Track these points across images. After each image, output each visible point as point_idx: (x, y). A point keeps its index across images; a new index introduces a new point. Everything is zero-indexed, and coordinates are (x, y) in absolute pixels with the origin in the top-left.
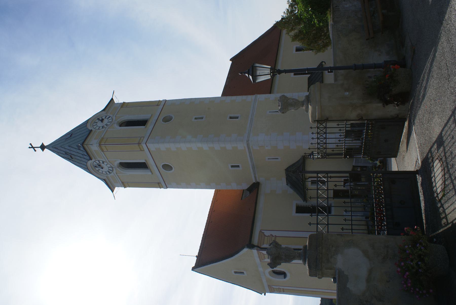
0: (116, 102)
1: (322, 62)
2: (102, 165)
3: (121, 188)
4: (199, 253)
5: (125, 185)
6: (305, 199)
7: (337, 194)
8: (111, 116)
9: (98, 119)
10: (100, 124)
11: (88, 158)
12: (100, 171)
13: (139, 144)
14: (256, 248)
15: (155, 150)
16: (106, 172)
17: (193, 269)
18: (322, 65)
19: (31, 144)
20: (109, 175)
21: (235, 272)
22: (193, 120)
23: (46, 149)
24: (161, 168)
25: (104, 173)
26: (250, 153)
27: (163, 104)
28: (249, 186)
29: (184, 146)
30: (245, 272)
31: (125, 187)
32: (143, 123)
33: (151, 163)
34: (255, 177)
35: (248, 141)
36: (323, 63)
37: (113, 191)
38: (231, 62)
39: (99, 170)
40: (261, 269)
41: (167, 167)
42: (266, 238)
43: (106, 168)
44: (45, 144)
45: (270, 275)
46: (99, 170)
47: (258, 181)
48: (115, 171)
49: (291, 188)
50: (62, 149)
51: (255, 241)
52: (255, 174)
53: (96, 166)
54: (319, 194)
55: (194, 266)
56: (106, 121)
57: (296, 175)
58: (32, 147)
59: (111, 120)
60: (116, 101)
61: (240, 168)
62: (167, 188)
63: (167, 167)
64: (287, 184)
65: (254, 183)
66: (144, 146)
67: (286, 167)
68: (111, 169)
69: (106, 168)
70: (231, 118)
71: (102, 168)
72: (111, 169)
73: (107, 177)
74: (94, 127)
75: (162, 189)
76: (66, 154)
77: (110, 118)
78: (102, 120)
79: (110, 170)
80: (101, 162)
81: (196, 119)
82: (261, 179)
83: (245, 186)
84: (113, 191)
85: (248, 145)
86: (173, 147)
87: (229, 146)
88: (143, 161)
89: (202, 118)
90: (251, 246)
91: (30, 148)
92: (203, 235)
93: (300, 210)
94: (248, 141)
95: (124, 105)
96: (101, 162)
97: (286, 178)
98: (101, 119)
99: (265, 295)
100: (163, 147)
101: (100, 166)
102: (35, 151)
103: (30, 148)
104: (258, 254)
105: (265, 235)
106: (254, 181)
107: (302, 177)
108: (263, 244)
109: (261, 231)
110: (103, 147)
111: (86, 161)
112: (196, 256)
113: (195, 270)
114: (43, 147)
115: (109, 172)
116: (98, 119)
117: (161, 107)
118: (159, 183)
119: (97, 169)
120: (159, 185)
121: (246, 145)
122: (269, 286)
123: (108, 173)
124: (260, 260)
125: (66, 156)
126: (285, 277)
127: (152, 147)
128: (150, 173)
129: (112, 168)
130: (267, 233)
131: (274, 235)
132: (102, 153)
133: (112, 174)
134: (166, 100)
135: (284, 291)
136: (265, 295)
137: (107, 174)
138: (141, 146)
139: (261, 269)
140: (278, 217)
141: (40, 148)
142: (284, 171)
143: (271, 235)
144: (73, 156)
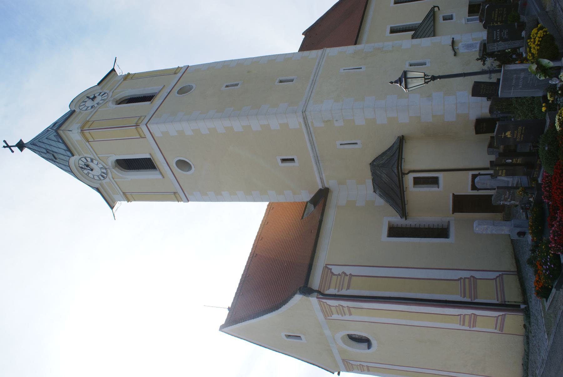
0: (119, 75)
1: (435, 7)
2: (92, 165)
3: (122, 202)
4: (233, 303)
5: (128, 197)
6: (404, 214)
7: (461, 204)
8: (107, 91)
9: (88, 97)
10: (89, 103)
11: (69, 153)
12: (90, 175)
13: (137, 125)
14: (316, 294)
15: (160, 135)
16: (98, 176)
17: (222, 328)
18: (434, 12)
19: (5, 141)
20: (104, 181)
21: (288, 336)
22: (224, 88)
23: (26, 150)
24: (176, 167)
25: (96, 178)
26: (309, 134)
27: (183, 70)
28: (312, 195)
29: (204, 126)
30: (302, 336)
31: (128, 200)
32: (148, 98)
33: (158, 159)
34: (321, 179)
35: (304, 112)
36: (436, 9)
37: (112, 208)
38: (304, 36)
39: (89, 173)
40: (327, 332)
41: (183, 165)
42: (334, 278)
43: (97, 171)
44: (25, 141)
45: (344, 342)
46: (89, 173)
47: (327, 186)
48: (110, 175)
49: (380, 196)
50: (40, 144)
51: (316, 282)
52: (320, 173)
53: (82, 168)
54: (427, 203)
55: (223, 323)
56: (98, 99)
57: (389, 173)
58: (8, 146)
59: (105, 98)
60: (119, 72)
61: (296, 164)
62: (188, 201)
63: (183, 165)
64: (375, 191)
65: (320, 190)
66: (144, 128)
67: (370, 161)
68: (104, 171)
69: (97, 171)
70: (281, 82)
71: (92, 170)
72: (104, 171)
73: (100, 184)
74: (81, 108)
75: (181, 203)
76: (48, 152)
77: (106, 94)
78: (94, 99)
79: (103, 173)
80: (89, 160)
81: (227, 86)
82: (329, 184)
83: (306, 197)
84: (112, 208)
85: (305, 119)
86: (188, 128)
87: (274, 123)
88: (147, 156)
89: (237, 85)
90: (307, 291)
91: (4, 147)
92: (243, 275)
93: (395, 232)
94: (304, 112)
95: (128, 77)
96: (89, 160)
97: (373, 180)
98: (92, 97)
99: (339, 374)
100: (173, 129)
101: (88, 166)
102: (13, 152)
103: (4, 147)
104: (320, 305)
105: (332, 273)
106: (320, 187)
107: (396, 171)
108: (329, 288)
109: (326, 267)
110: (86, 132)
111: (68, 158)
112: (229, 308)
113: (223, 330)
114: (21, 146)
115: (102, 176)
116: (88, 97)
117: (179, 75)
118: (175, 193)
119: (86, 172)
120: (175, 196)
121: (301, 120)
122: (343, 360)
123: (102, 178)
124: (325, 316)
125: (48, 156)
126: (369, 346)
127: (158, 129)
128: (160, 177)
129: (106, 169)
130: (336, 270)
131: (348, 273)
132: (87, 143)
133: (107, 180)
134: (188, 66)
135: (369, 370)
136: (339, 374)
137: (100, 179)
138: (139, 129)
139: (327, 332)
140: (355, 238)
141: (17, 148)
142: (369, 168)
143: (344, 273)
144: (55, 154)
